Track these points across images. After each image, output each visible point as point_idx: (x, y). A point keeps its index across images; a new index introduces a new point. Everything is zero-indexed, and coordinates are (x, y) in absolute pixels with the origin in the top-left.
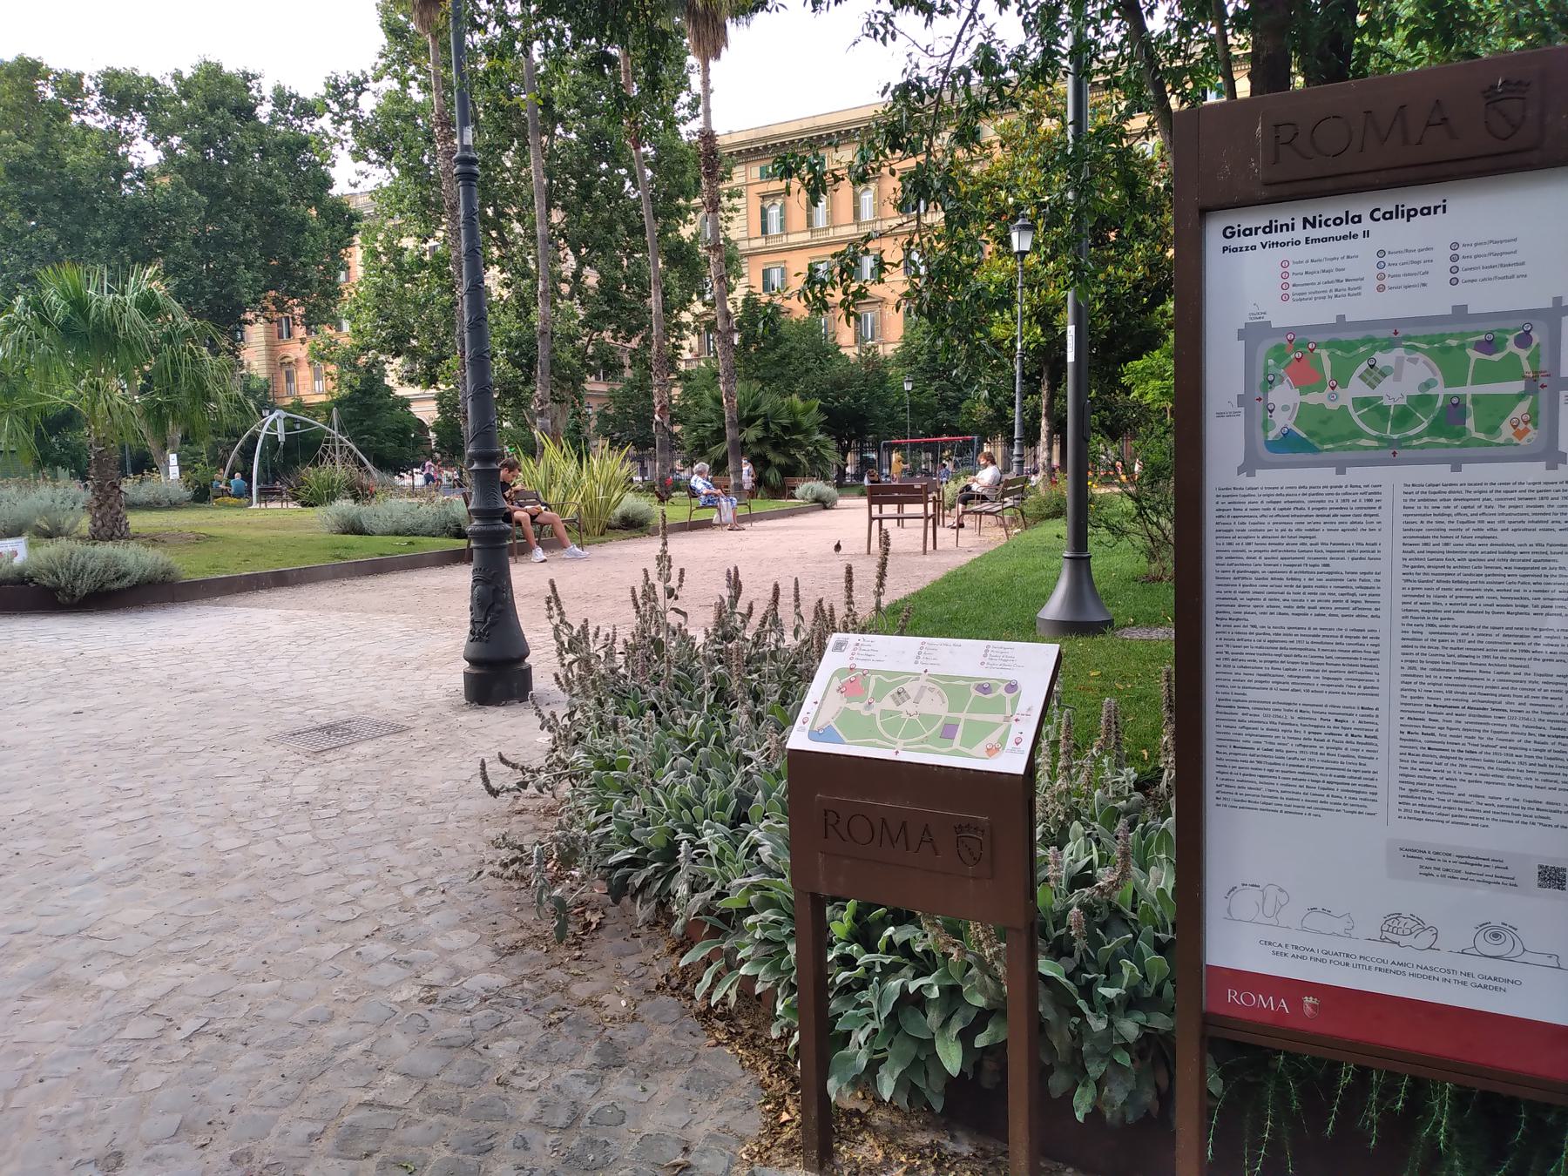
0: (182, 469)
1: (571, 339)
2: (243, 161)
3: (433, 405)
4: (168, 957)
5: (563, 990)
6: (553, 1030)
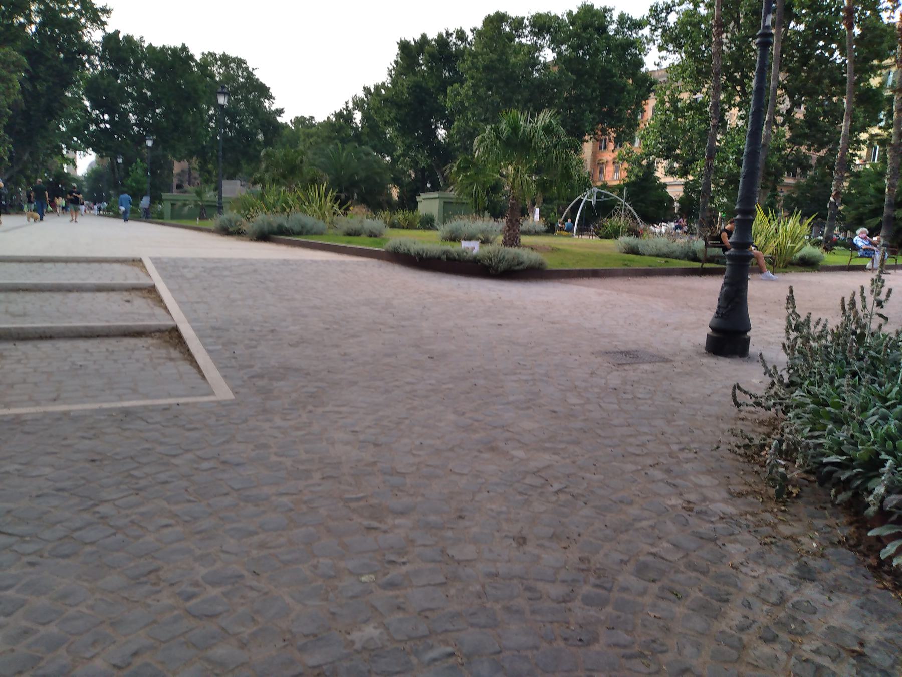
0: (541, 216)
1: (779, 150)
2: (597, 56)
3: (681, 188)
4: (545, 450)
5: (774, 526)
6: (767, 547)
